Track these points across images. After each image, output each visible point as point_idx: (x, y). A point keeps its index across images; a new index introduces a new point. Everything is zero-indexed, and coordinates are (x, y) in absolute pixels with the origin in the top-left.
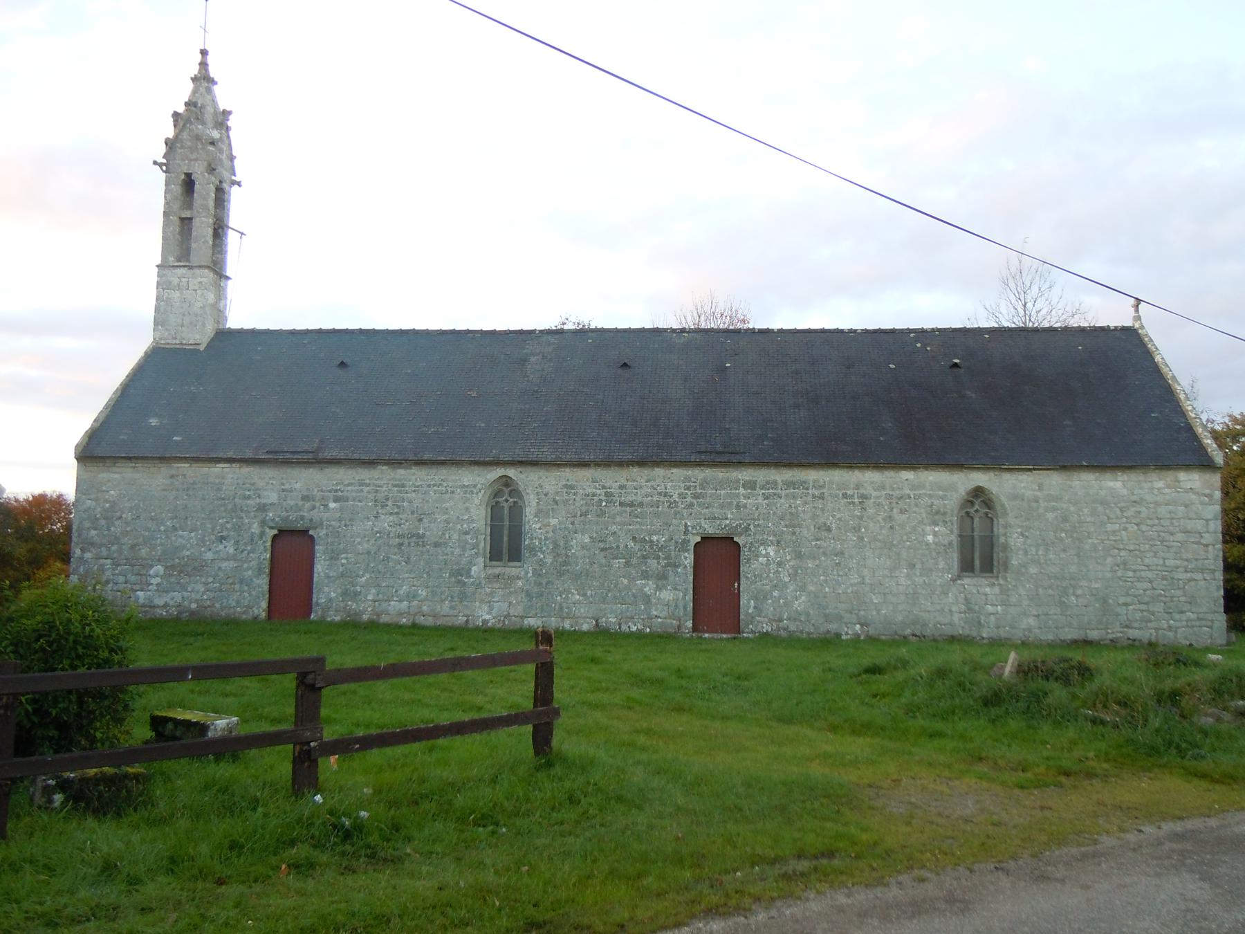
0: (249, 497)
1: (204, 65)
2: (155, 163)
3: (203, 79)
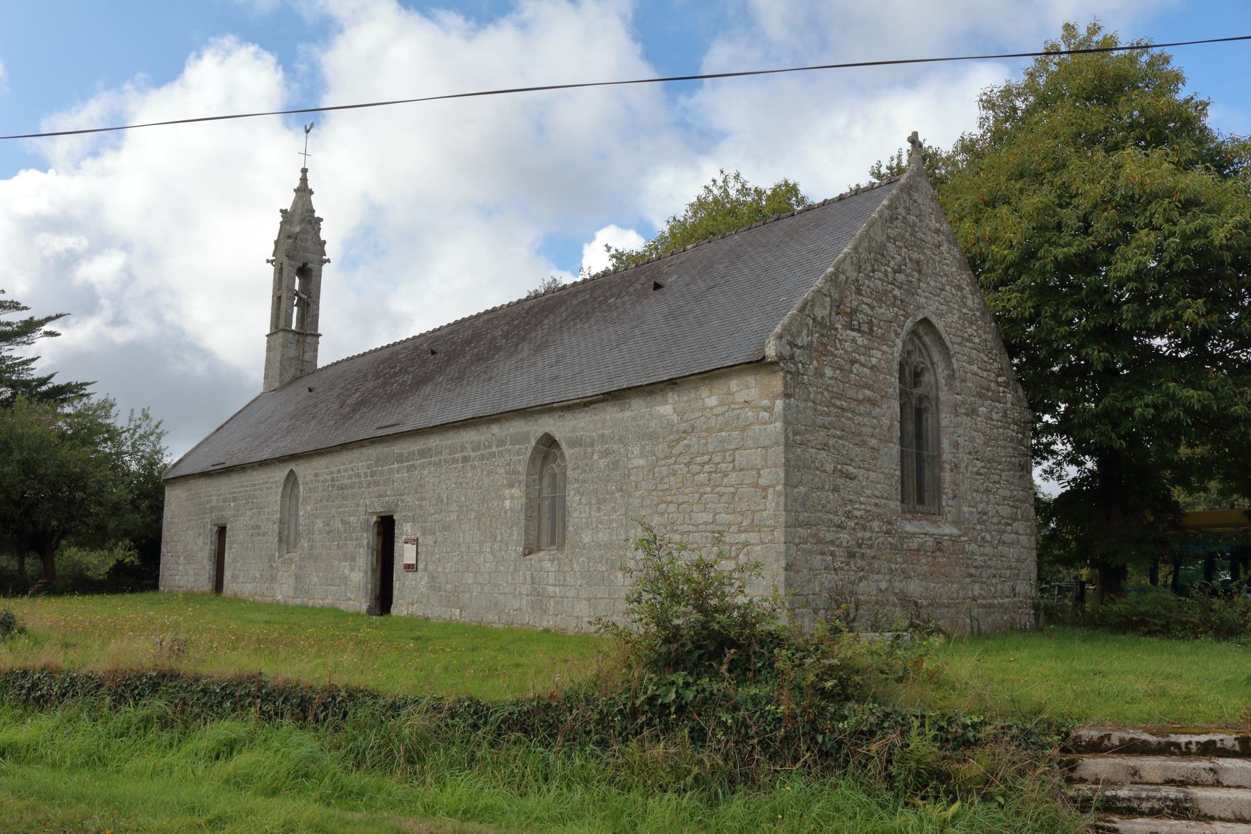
0: (840, 527)
1: (304, 180)
2: (268, 261)
3: (304, 191)
